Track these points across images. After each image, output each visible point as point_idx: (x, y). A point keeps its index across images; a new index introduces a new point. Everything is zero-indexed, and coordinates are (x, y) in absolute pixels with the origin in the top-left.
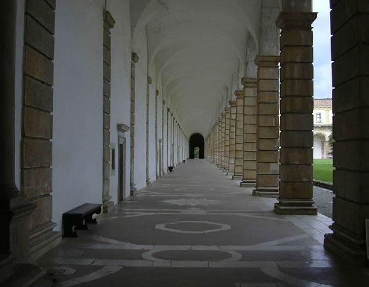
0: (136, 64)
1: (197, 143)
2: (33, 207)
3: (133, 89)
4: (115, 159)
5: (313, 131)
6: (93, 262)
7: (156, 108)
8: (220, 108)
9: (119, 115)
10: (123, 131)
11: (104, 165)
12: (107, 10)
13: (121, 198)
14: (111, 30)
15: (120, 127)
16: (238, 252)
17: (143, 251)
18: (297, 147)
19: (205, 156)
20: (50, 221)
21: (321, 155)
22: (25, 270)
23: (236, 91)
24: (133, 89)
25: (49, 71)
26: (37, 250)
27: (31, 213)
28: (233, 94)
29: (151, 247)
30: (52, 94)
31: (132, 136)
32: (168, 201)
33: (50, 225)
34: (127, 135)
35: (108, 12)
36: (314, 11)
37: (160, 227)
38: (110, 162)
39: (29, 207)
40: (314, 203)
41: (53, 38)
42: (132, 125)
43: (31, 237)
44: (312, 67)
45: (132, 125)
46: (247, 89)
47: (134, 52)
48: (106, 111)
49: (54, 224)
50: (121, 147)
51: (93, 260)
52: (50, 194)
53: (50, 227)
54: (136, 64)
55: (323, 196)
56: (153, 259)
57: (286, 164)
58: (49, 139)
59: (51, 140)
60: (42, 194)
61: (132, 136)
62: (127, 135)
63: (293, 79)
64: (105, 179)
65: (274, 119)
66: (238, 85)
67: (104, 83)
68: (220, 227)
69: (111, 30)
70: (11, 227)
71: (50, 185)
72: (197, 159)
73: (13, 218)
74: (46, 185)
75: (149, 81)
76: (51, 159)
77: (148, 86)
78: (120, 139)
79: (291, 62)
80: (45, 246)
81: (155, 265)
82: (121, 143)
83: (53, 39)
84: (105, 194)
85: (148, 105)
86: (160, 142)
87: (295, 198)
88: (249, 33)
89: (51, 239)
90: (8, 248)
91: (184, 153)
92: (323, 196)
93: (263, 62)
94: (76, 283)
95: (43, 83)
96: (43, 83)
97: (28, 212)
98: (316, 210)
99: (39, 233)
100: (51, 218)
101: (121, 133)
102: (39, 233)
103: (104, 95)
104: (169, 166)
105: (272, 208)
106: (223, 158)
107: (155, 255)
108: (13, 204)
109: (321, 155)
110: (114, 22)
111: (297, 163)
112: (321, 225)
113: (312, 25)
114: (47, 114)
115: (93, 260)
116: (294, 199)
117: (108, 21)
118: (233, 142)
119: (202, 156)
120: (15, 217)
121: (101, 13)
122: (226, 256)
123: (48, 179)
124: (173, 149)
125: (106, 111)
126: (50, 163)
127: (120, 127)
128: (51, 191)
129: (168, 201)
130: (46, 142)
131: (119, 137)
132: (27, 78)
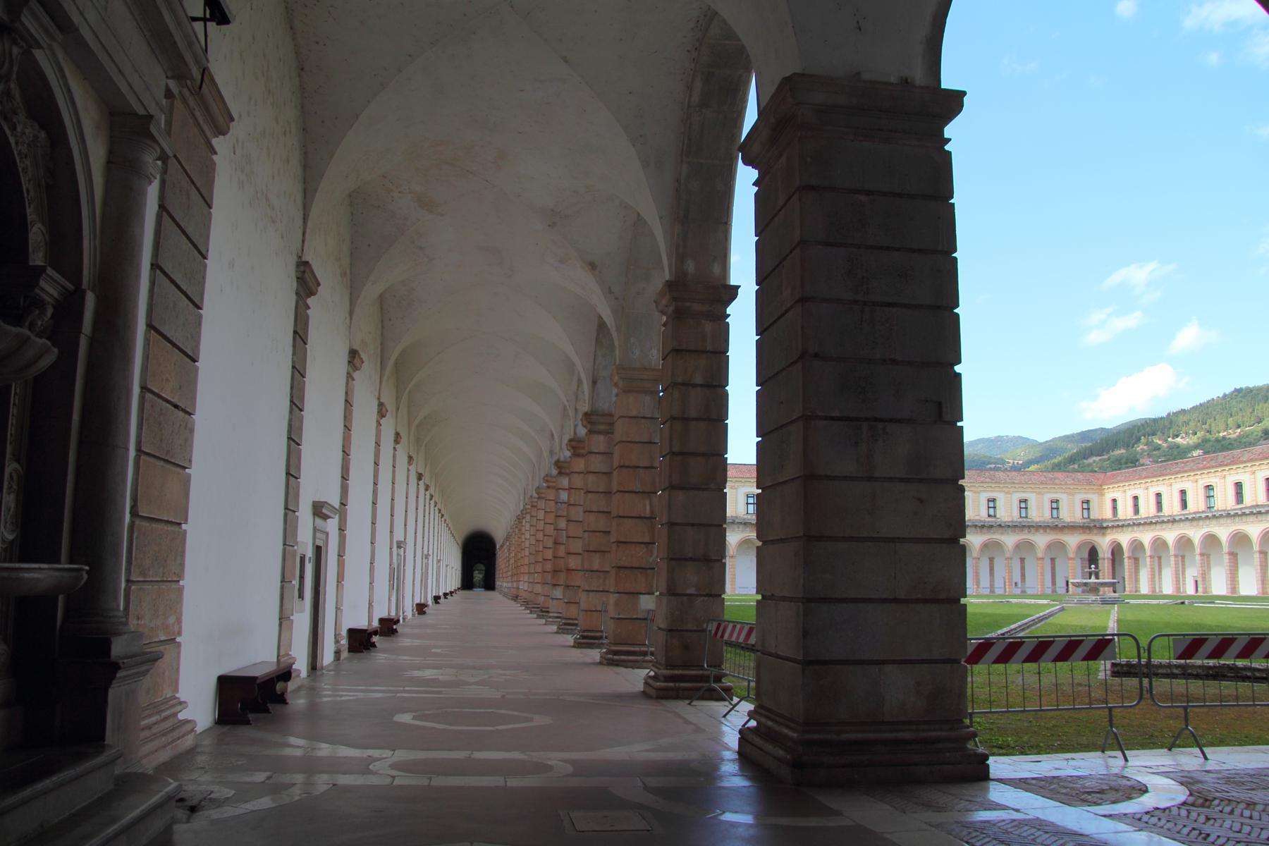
0: (356, 375)
1: (479, 557)
2: (157, 658)
3: (347, 428)
4: (306, 576)
5: (759, 597)
6: (269, 778)
7: (394, 472)
8: (399, 565)
9: (319, 482)
10: (325, 517)
11: (282, 588)
12: (306, 258)
13: (314, 666)
14: (310, 301)
15: (319, 510)
16: (565, 761)
17: (372, 760)
18: (691, 559)
19: (498, 583)
20: (174, 698)
21: (741, 581)
22: (130, 783)
23: (570, 440)
24: (347, 428)
25: (189, 384)
26: (152, 753)
27: (148, 671)
28: (564, 447)
29: (387, 753)
30: (192, 431)
31: (342, 529)
32: (417, 673)
33: (173, 706)
34: (332, 525)
35: (306, 263)
36: (733, 282)
37: (406, 718)
38: (296, 582)
39: (148, 659)
40: (726, 675)
41: (200, 316)
42: (343, 504)
43: (143, 723)
44: (725, 396)
45: (343, 504)
46: (595, 437)
47: (355, 347)
48: (292, 474)
49: (181, 703)
50: (318, 550)
51: (267, 774)
52: (178, 639)
53: (173, 710)
54: (356, 375)
55: (739, 669)
56: (394, 773)
57: (672, 591)
58: (180, 524)
59: (184, 527)
60: (163, 638)
61: (342, 529)
62: (332, 525)
63: (686, 420)
64: (284, 619)
65: (647, 503)
66: (576, 426)
67: (291, 412)
68: (531, 720)
69: (310, 301)
70: (112, 693)
71: (179, 621)
72: (479, 593)
73: (118, 675)
74: (172, 620)
75: (382, 413)
76: (182, 565)
77: (379, 424)
78: (318, 535)
79: (683, 384)
80: (164, 747)
81: (397, 782)
82: (319, 543)
83: (199, 320)
84: (282, 653)
85: (376, 464)
86: (399, 547)
87: (688, 674)
88: (600, 317)
89: (176, 734)
90: (103, 739)
91: (451, 577)
92: (739, 669)
93: (632, 381)
94: (239, 811)
95: (176, 406)
96: (176, 406)
97: (144, 668)
98: (728, 690)
99: (154, 719)
100: (176, 690)
101: (319, 521)
102: (154, 719)
103: (290, 438)
104: (417, 601)
105: (640, 687)
106: (538, 588)
107: (394, 766)
108: (118, 648)
109: (741, 581)
110: (319, 284)
111: (692, 591)
112: (733, 721)
113: (729, 311)
114: (181, 471)
115: (267, 774)
116: (685, 666)
117: (306, 284)
118: (562, 550)
119: (489, 585)
120: (120, 674)
121: (292, 261)
122: (543, 768)
123: (175, 605)
124: (427, 565)
125: (292, 474)
126: (180, 575)
127: (319, 510)
128: (180, 633)
129: (417, 673)
130: (176, 529)
131: (315, 530)
132: (148, 395)
